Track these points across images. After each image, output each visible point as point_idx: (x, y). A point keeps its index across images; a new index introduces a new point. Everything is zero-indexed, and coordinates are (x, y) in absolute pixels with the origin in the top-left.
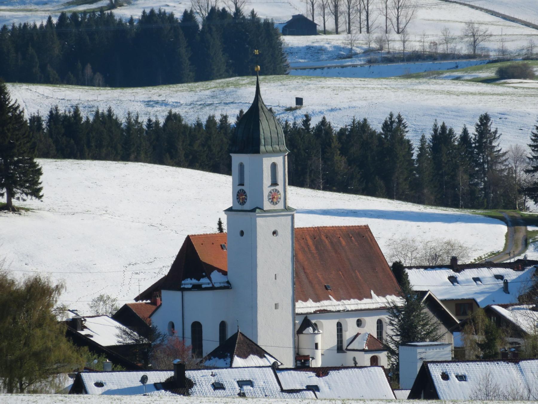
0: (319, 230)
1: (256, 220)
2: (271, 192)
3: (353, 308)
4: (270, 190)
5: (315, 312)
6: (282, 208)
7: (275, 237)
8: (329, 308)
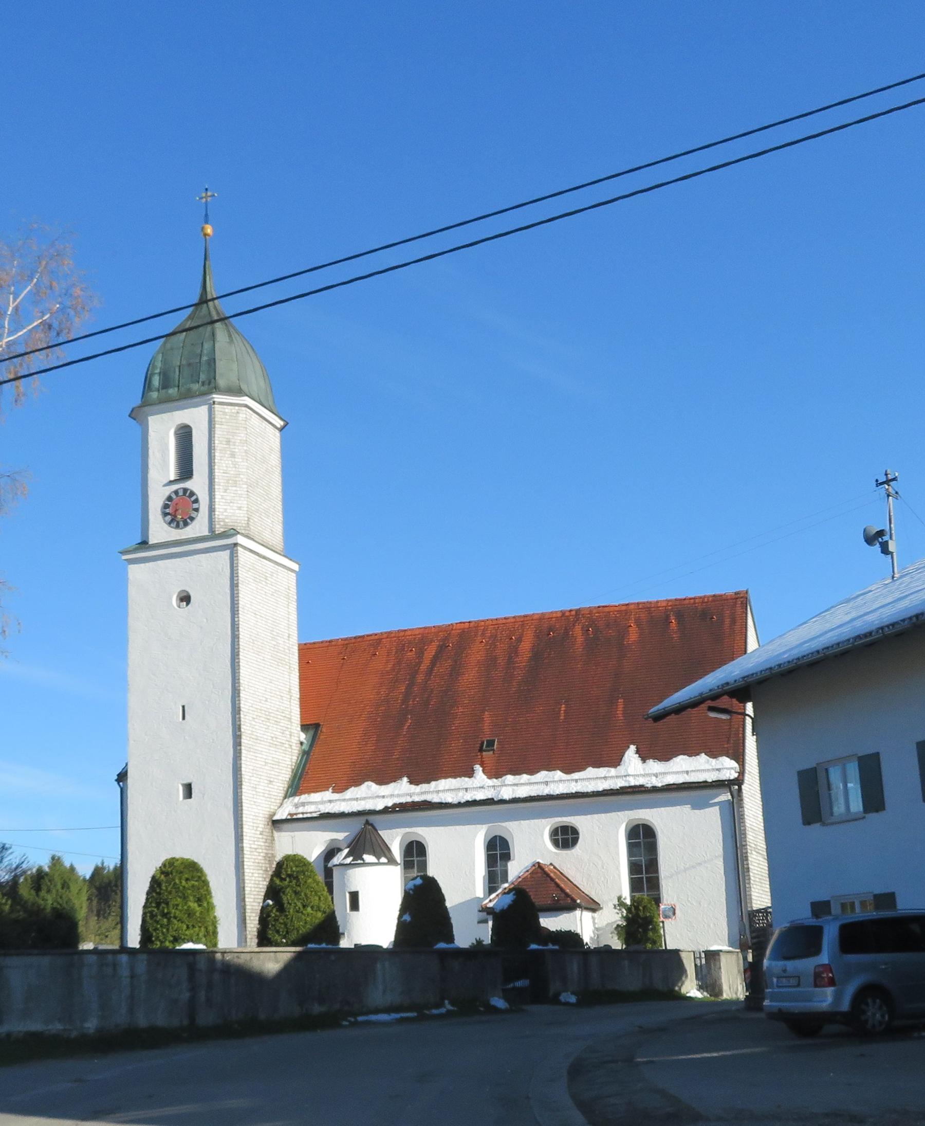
0: (302, 649)
1: (402, 928)
2: (169, 498)
3: (522, 792)
4: (167, 494)
5: (386, 810)
6: (206, 533)
7: (185, 610)
8: (436, 799)
